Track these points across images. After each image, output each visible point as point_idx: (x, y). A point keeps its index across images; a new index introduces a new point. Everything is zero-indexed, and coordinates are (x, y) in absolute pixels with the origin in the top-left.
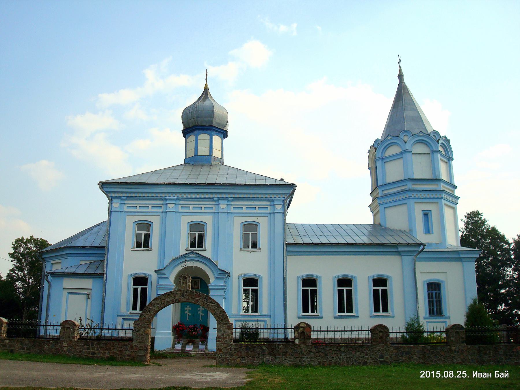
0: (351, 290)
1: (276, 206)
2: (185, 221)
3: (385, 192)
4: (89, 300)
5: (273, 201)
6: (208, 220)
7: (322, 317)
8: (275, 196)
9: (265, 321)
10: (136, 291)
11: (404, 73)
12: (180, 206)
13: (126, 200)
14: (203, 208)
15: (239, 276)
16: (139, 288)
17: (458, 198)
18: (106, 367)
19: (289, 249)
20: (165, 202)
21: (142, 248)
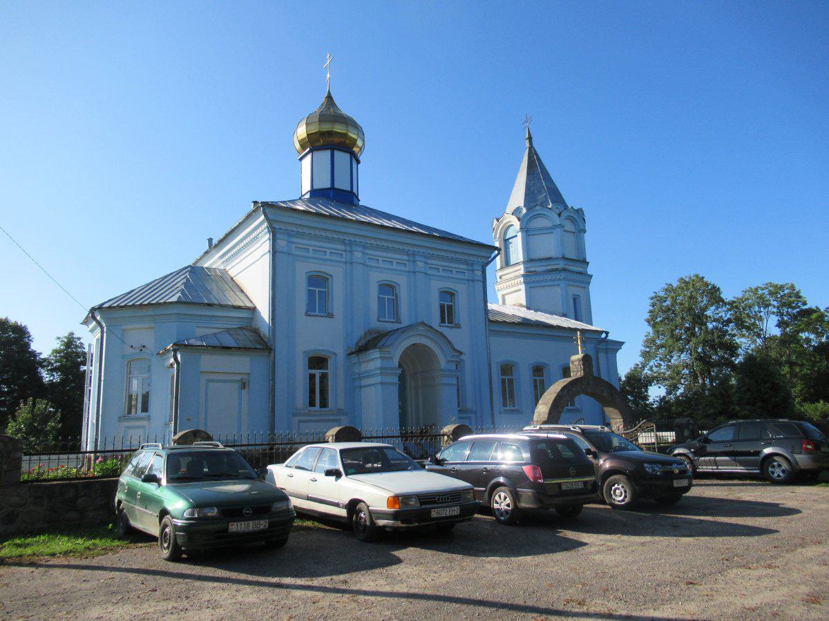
0: (328, 373)
1: (418, 263)
2: (436, 286)
3: (567, 267)
4: (244, 392)
5: (414, 255)
6: (402, 281)
7: (522, 412)
8: (475, 259)
9: (143, 427)
10: (312, 377)
11: (532, 136)
12: (294, 245)
13: (294, 236)
14: (394, 264)
15: (305, 352)
16: (317, 373)
17: (591, 276)
18: (440, 489)
19: (493, 328)
20: (411, 258)
21: (446, 324)
